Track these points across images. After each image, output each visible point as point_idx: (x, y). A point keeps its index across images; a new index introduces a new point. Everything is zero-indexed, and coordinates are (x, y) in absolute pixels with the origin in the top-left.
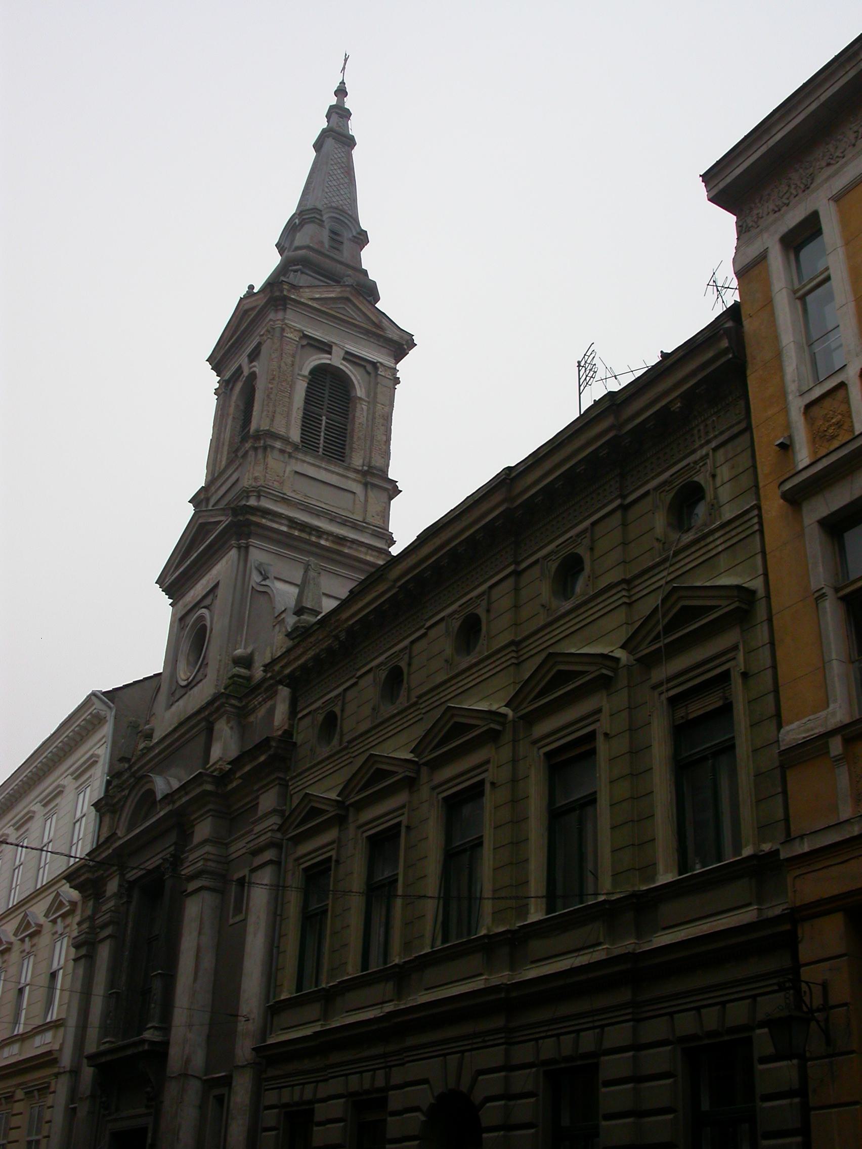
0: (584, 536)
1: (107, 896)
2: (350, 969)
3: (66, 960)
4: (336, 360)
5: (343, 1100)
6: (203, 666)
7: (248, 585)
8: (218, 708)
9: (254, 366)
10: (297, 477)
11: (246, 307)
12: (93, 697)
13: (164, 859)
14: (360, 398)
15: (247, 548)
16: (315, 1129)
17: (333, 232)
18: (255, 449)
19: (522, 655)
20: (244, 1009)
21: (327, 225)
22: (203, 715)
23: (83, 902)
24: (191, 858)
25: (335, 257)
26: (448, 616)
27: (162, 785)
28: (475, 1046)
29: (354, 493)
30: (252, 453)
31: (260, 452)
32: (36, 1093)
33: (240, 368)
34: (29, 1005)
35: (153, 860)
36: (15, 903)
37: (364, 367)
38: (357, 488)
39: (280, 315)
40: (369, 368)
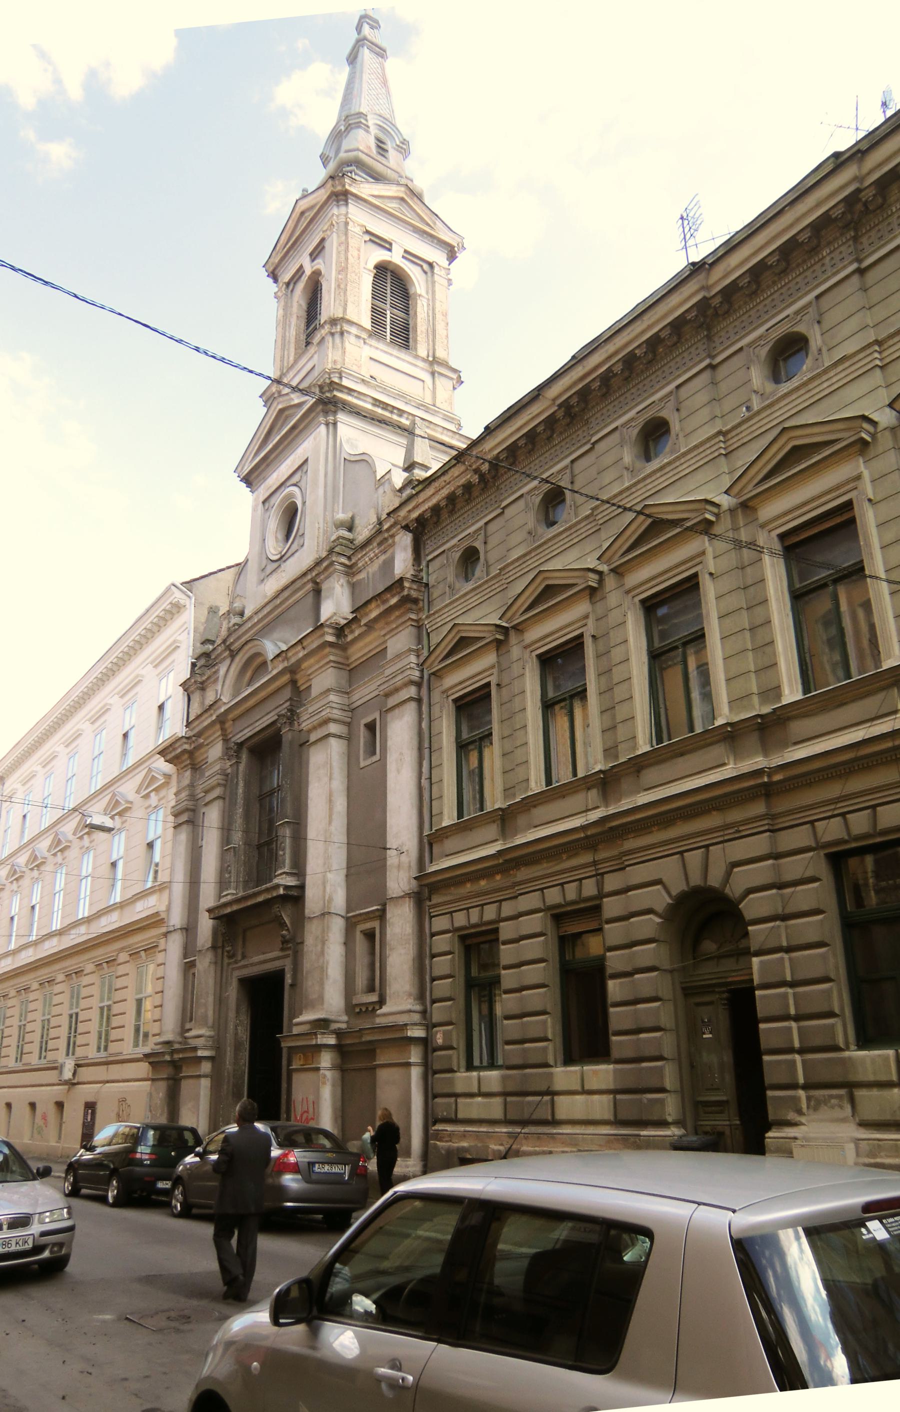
0: (806, 311)
1: (209, 762)
2: (532, 784)
3: (165, 829)
4: (396, 257)
5: (541, 914)
6: (298, 536)
7: (340, 459)
8: (326, 568)
9: (319, 264)
10: (372, 362)
11: (302, 209)
12: (173, 587)
13: (278, 716)
14: (420, 296)
15: (335, 424)
16: (502, 947)
17: (379, 140)
18: (332, 334)
19: (730, 445)
20: (392, 842)
21: (373, 130)
22: (309, 577)
23: (178, 774)
24: (310, 710)
25: (383, 162)
26: (622, 426)
27: (270, 648)
28: (726, 838)
29: (423, 381)
30: (329, 339)
31: (337, 337)
32: (105, 965)
33: (300, 270)
34: (39, 918)
35: (262, 721)
36: (98, 788)
37: (422, 266)
38: (427, 377)
39: (343, 210)
40: (425, 266)
